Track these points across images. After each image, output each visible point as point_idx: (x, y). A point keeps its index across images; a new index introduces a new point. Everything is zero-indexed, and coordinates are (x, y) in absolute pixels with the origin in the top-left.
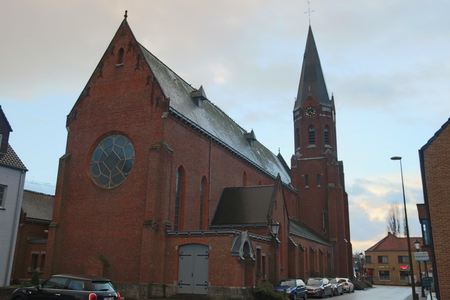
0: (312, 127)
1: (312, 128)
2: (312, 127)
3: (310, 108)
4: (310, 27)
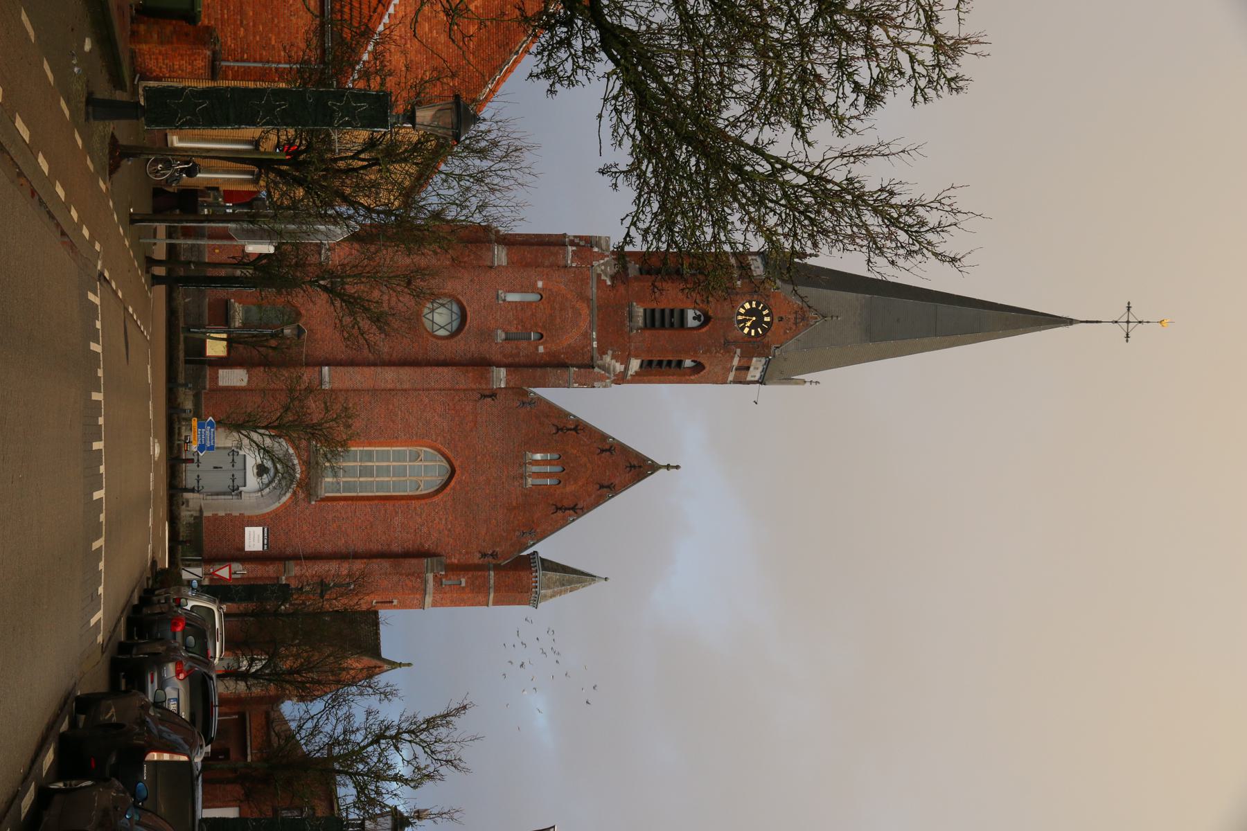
0: (702, 318)
1: (696, 318)
2: (702, 318)
3: (767, 319)
4: (1069, 322)
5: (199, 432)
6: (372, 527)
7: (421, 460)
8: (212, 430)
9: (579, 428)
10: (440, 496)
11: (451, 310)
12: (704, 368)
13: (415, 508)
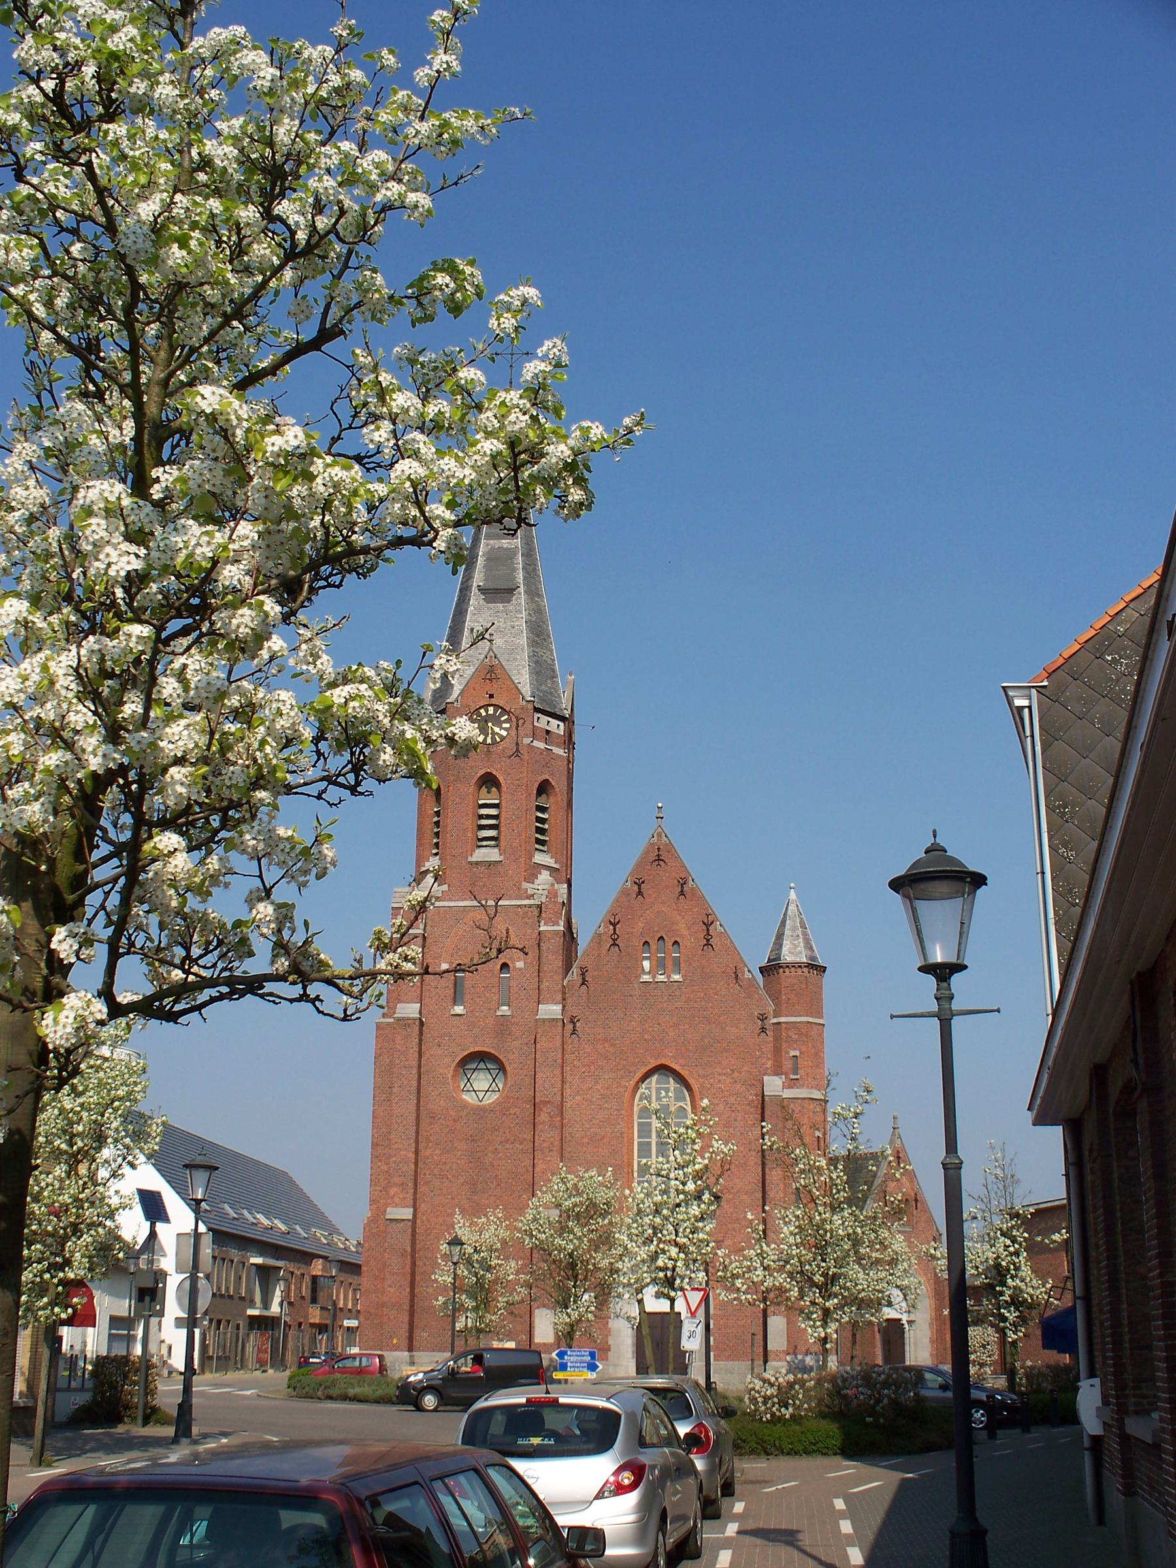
10: (691, 1081)
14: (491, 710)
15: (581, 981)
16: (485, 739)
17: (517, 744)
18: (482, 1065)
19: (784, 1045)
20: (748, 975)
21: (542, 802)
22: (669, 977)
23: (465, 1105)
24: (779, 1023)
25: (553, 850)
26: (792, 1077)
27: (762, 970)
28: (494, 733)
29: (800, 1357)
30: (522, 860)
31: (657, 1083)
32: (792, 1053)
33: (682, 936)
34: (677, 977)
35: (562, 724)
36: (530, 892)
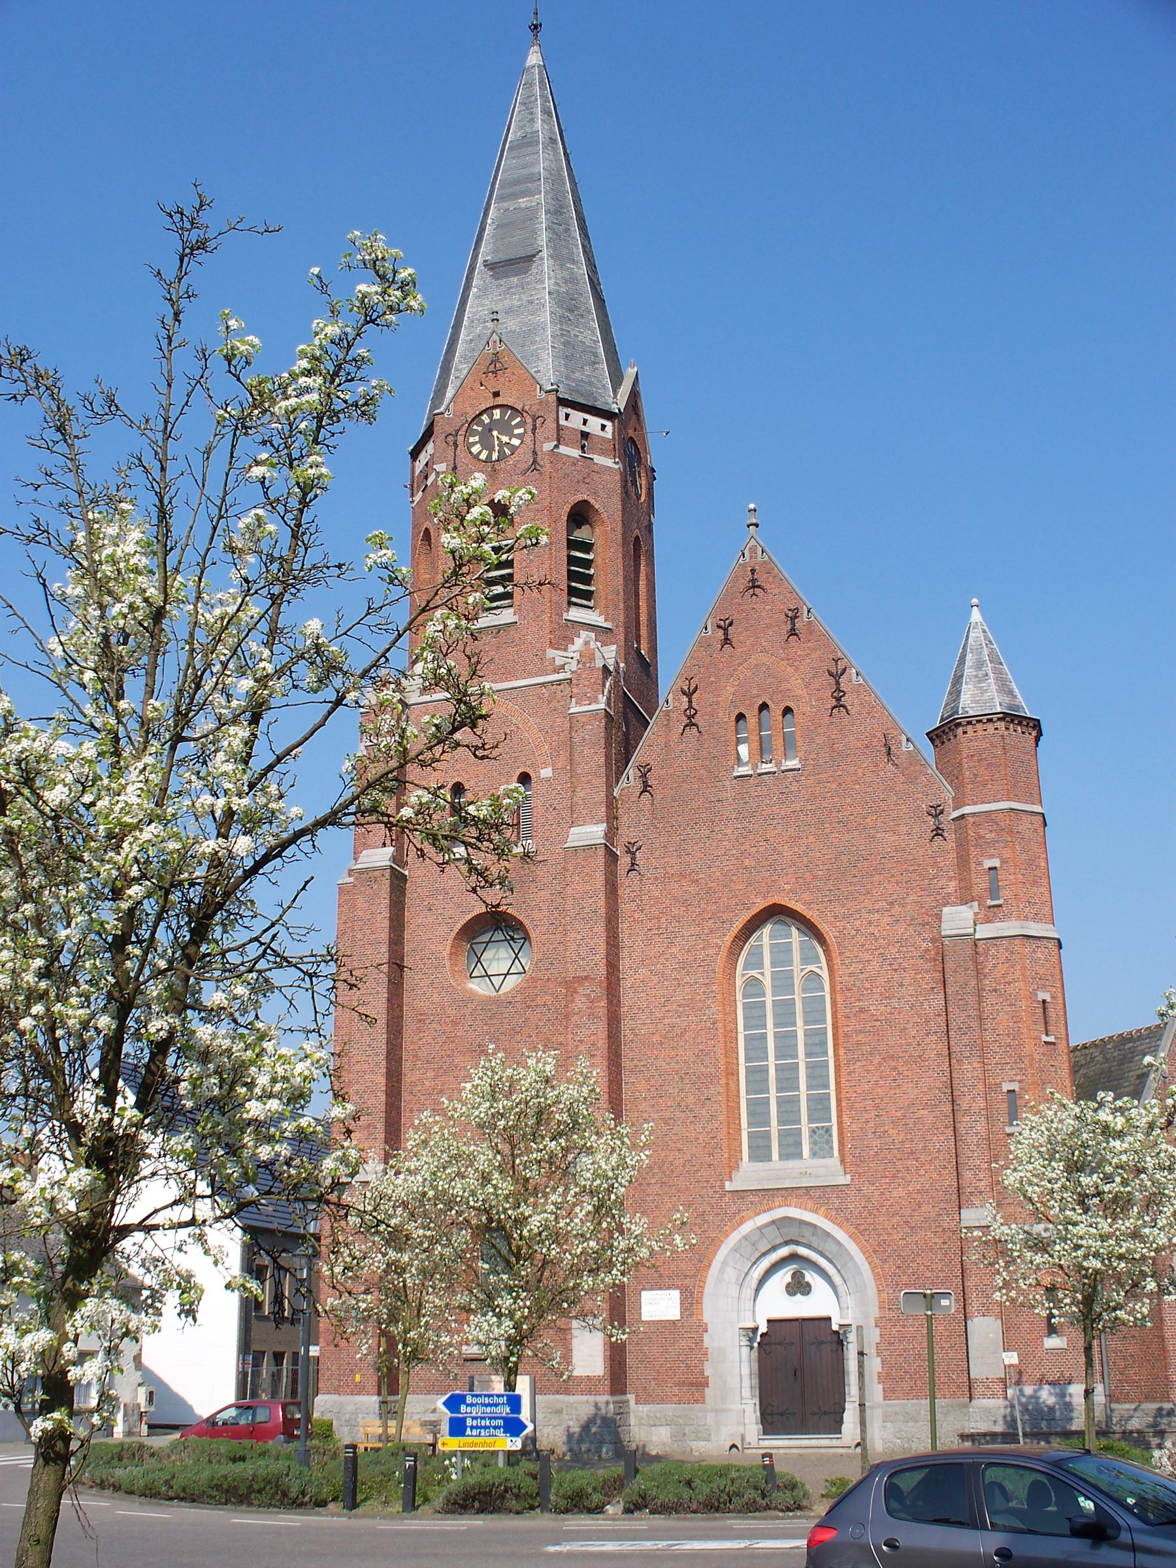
5: (475, 1432)
6: (892, 1057)
7: (762, 974)
8: (469, 1400)
9: (686, 688)
10: (824, 928)
11: (488, 943)
12: (584, 504)
13: (851, 975)
14: (497, 414)
15: (640, 787)
16: (490, 456)
17: (535, 453)
18: (499, 936)
19: (973, 852)
20: (906, 747)
21: (582, 534)
22: (778, 764)
23: (471, 997)
24: (962, 817)
25: (602, 602)
26: (990, 902)
27: (934, 736)
28: (501, 444)
29: (1028, 1390)
30: (546, 617)
31: (771, 937)
32: (988, 863)
33: (797, 698)
34: (793, 763)
35: (608, 424)
36: (559, 662)
